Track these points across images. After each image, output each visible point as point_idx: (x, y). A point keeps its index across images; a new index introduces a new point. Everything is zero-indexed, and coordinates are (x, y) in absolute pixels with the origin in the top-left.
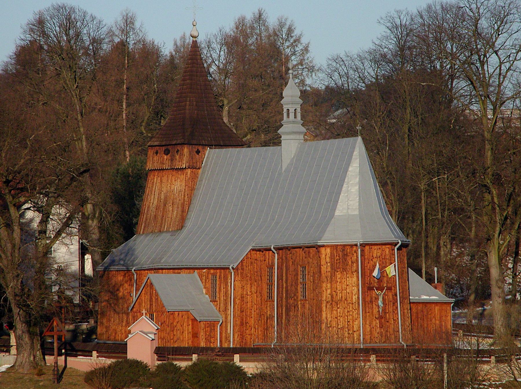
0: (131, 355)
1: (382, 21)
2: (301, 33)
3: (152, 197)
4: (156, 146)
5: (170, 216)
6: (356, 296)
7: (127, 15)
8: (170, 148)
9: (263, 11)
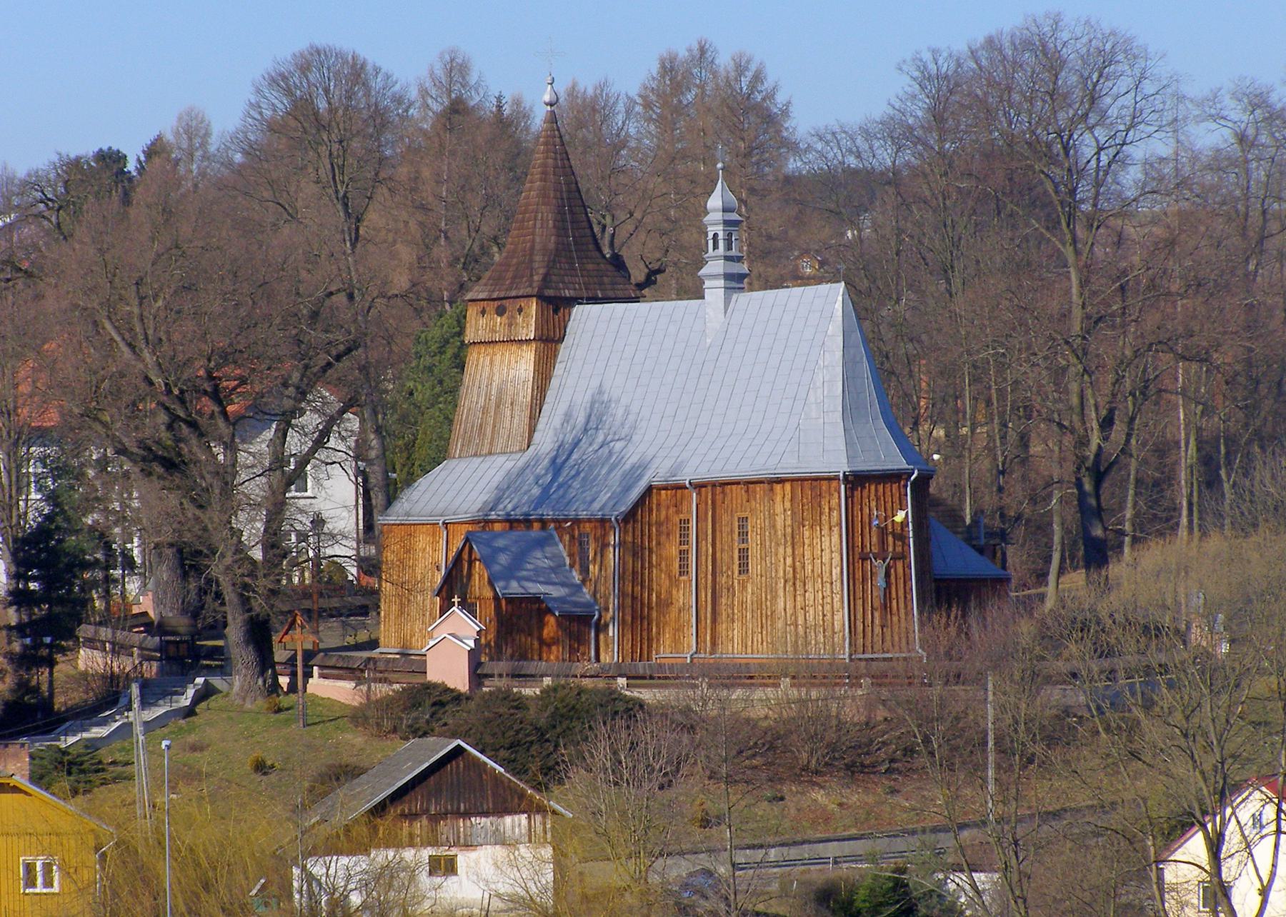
0: (433, 676)
1: (904, 67)
5: (507, 424)
6: (839, 569)
9: (707, 46)
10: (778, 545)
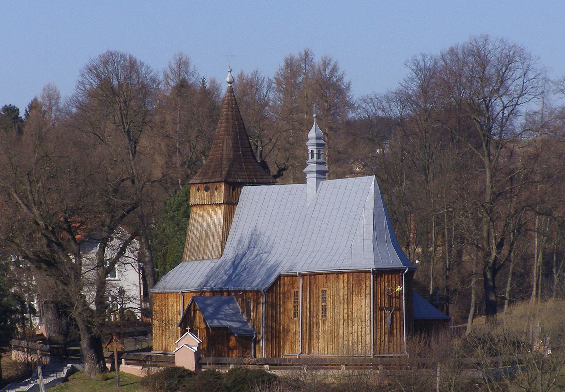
2: (343, 73)
3: (195, 229)
4: (198, 183)
5: (211, 245)
6: (369, 315)
7: (180, 59)
8: (209, 185)
10: (340, 303)
